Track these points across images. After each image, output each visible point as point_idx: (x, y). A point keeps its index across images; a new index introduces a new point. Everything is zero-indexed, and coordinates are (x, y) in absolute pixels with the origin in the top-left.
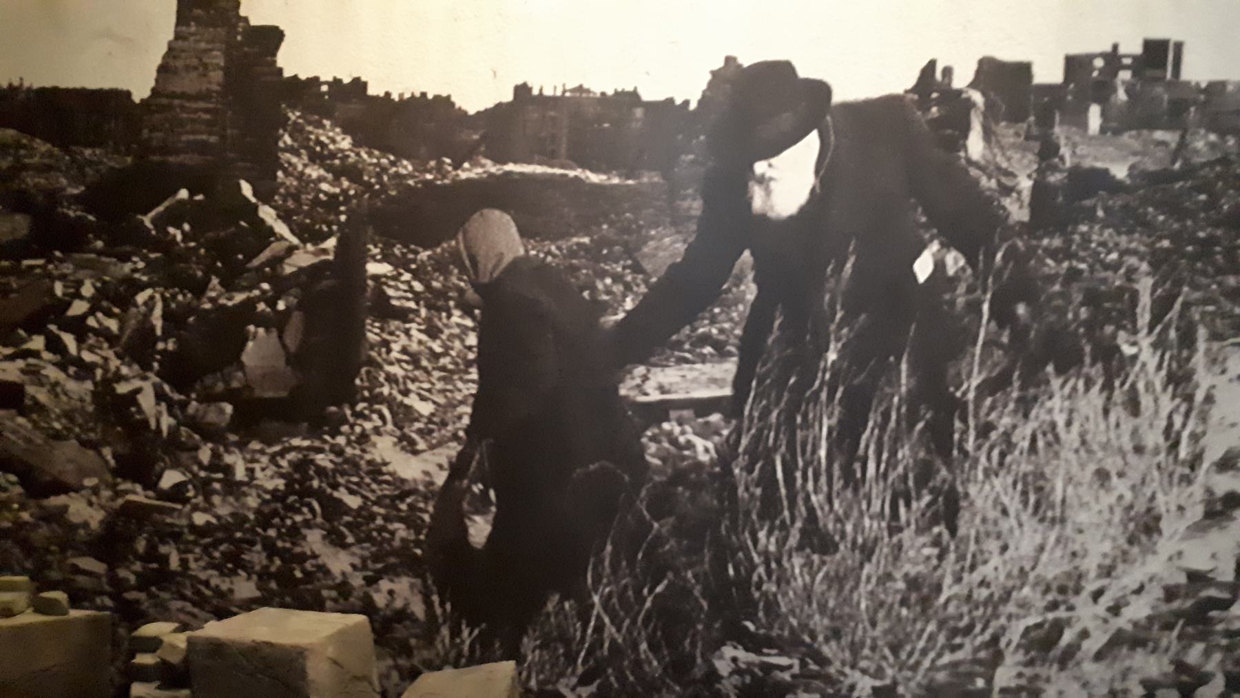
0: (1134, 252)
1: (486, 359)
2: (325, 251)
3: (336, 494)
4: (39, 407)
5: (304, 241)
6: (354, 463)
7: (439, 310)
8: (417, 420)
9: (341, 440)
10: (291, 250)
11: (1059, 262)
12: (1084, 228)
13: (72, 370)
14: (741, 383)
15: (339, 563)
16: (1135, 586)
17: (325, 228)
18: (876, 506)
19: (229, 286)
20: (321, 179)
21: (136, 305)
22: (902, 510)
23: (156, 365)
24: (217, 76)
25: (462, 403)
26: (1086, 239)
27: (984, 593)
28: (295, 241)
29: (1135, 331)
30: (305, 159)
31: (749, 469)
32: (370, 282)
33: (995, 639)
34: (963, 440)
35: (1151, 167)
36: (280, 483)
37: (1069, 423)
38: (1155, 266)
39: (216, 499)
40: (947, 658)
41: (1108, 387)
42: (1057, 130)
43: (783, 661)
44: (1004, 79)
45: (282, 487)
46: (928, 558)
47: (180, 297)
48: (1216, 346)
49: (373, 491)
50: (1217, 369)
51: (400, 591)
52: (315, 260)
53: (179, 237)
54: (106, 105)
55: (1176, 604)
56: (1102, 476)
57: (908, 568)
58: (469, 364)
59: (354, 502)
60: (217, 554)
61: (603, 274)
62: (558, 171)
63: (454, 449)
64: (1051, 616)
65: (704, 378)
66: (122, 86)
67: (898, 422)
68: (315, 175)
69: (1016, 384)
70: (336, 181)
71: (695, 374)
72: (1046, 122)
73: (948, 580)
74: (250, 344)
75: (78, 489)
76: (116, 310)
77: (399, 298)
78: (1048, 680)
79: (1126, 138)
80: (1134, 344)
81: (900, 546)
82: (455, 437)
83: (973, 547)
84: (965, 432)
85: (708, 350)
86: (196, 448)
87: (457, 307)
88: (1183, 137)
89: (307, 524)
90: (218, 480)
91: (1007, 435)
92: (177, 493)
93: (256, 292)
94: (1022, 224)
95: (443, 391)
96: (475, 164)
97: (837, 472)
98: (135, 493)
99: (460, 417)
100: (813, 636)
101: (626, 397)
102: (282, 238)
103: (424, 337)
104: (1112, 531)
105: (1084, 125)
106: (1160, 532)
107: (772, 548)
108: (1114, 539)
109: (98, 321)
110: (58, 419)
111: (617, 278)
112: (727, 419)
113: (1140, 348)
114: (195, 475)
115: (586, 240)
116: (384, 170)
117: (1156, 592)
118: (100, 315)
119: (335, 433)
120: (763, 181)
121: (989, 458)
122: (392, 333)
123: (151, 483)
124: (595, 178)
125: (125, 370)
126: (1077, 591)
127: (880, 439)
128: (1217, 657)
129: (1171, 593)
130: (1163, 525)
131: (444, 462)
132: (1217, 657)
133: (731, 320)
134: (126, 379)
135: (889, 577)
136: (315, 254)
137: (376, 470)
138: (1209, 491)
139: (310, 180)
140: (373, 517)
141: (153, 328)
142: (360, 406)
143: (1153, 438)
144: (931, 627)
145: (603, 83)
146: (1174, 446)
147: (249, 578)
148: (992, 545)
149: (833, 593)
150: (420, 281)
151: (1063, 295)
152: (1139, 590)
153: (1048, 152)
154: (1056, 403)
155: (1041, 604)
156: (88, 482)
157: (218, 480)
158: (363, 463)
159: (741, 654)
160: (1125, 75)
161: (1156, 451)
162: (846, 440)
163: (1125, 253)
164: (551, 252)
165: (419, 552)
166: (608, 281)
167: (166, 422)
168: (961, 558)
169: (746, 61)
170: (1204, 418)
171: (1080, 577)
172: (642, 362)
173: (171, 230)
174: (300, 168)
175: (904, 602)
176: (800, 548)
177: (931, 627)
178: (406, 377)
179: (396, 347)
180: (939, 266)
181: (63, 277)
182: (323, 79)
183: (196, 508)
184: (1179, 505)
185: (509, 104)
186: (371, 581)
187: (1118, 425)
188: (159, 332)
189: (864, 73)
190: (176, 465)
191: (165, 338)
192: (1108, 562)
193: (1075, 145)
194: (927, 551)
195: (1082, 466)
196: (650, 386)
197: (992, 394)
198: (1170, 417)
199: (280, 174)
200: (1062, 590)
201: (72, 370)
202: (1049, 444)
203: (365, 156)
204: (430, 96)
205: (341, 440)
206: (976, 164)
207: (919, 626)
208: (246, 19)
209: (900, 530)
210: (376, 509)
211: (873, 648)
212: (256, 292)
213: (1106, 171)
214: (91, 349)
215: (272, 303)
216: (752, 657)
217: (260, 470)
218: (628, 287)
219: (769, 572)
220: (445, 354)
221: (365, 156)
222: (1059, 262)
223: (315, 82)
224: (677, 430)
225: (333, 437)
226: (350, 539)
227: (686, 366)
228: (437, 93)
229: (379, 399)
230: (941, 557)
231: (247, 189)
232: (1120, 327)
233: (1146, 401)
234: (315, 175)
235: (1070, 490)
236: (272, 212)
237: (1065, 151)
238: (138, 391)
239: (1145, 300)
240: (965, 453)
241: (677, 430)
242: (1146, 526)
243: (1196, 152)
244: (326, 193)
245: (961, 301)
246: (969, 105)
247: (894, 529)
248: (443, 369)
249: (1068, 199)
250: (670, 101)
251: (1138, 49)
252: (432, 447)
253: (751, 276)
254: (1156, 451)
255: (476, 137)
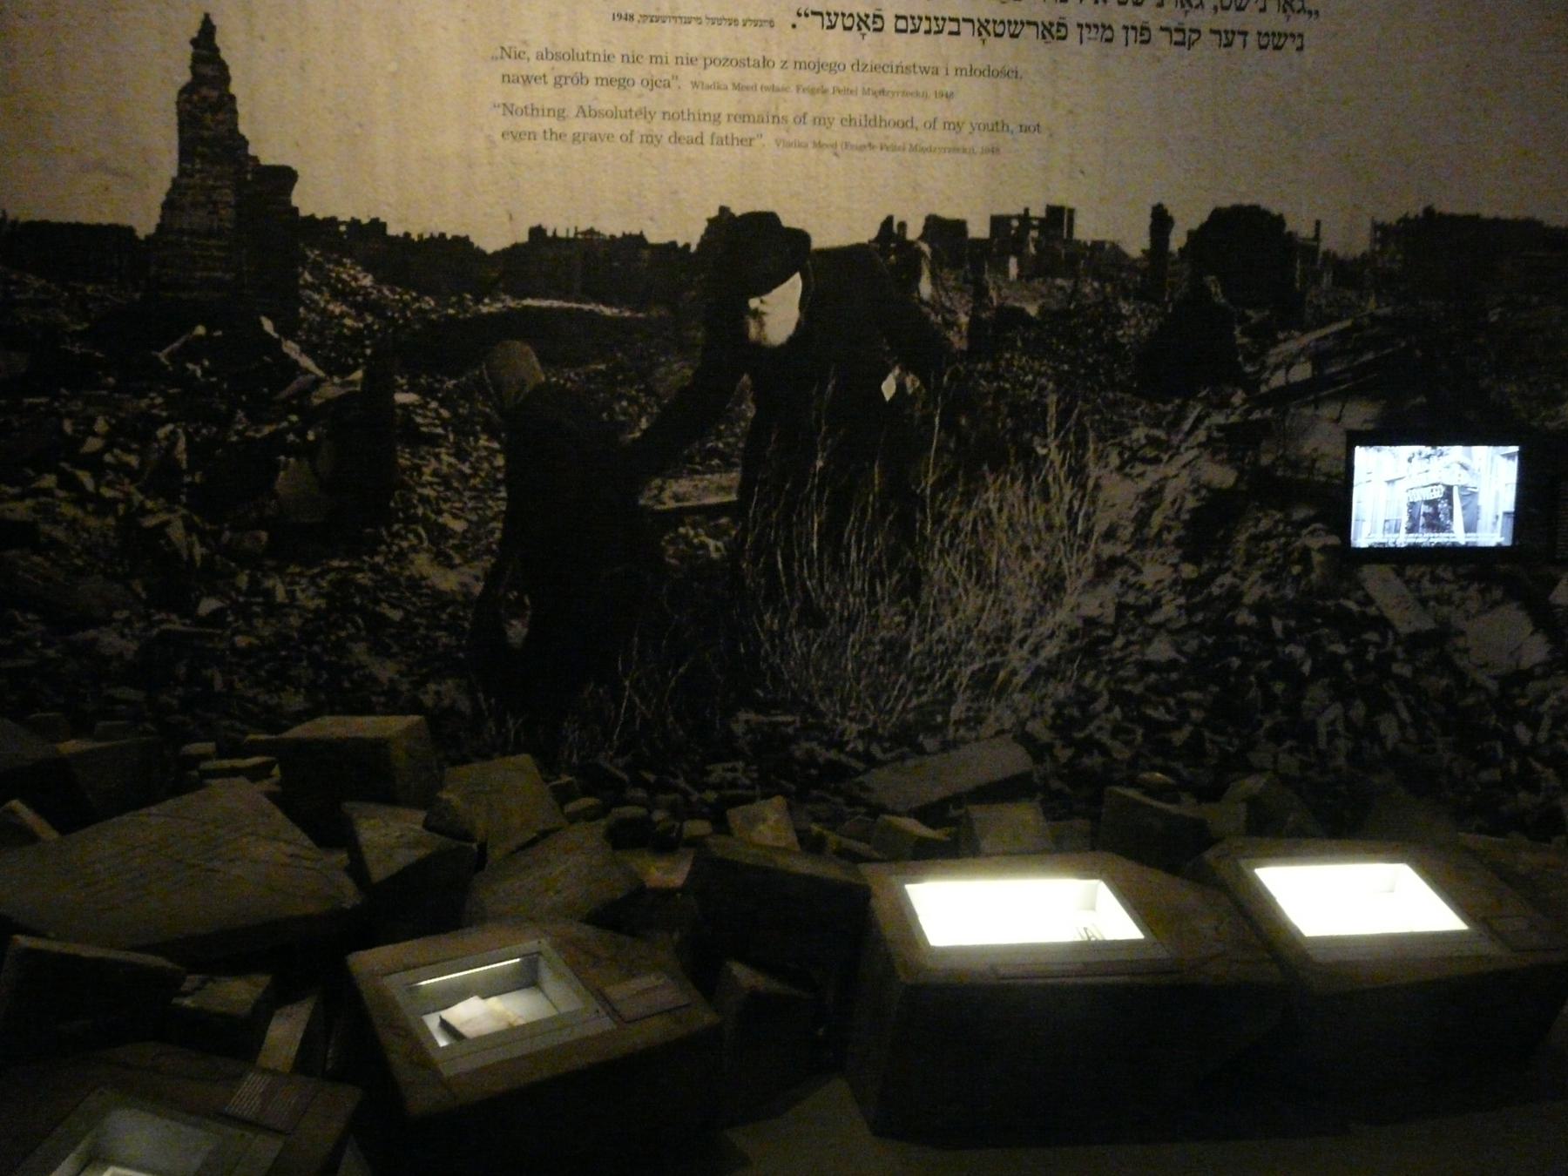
0: (1044, 375)
1: (513, 478)
2: (352, 383)
3: (441, 520)
4: (54, 542)
5: (330, 374)
6: (393, 580)
7: (466, 435)
8: (451, 537)
9: (379, 559)
10: (318, 382)
11: (990, 382)
12: (1008, 356)
13: (90, 507)
14: (745, 489)
15: (386, 671)
16: (1047, 633)
17: (351, 361)
18: (858, 585)
19: (255, 420)
20: (343, 315)
21: (156, 440)
22: (878, 588)
23: (183, 498)
24: (227, 213)
25: (494, 519)
26: (1009, 363)
27: (941, 648)
28: (321, 374)
29: (1046, 436)
30: (327, 296)
31: (755, 562)
32: (399, 411)
33: (950, 683)
34: (923, 527)
35: (1055, 307)
36: (321, 603)
37: (1000, 510)
38: (1059, 384)
39: (258, 623)
40: (914, 702)
41: (1027, 480)
42: (986, 276)
43: (789, 718)
44: (943, 231)
45: (323, 606)
46: (898, 625)
47: (204, 431)
48: (1101, 446)
49: (414, 604)
50: (1102, 464)
51: (446, 691)
52: (343, 392)
53: (199, 373)
54: (104, 244)
55: (1077, 643)
56: (1024, 549)
57: (883, 633)
58: (498, 483)
59: (396, 615)
60: (263, 673)
61: (621, 397)
62: (575, 305)
63: (488, 562)
64: (989, 662)
65: (713, 487)
66: (124, 220)
67: (873, 516)
68: (337, 311)
69: (961, 481)
70: (359, 317)
71: (705, 483)
72: (978, 270)
73: (914, 640)
74: (282, 474)
75: (108, 622)
76: (135, 446)
77: (427, 425)
78: (989, 710)
79: (1036, 283)
80: (1045, 446)
81: (877, 616)
82: (489, 551)
83: (931, 612)
84: (924, 522)
85: (715, 462)
86: (234, 574)
87: (484, 431)
88: (1076, 284)
89: (414, 549)
90: (258, 604)
91: (955, 521)
92: (216, 617)
93: (285, 424)
94: (962, 352)
95: (475, 509)
96: (494, 299)
97: (826, 560)
98: (169, 621)
99: (492, 532)
100: (811, 696)
101: (645, 506)
102: (307, 372)
103: (453, 460)
104: (1032, 592)
105: (1006, 272)
106: (1065, 590)
107: (775, 627)
108: (1034, 598)
109: (116, 457)
110: (79, 555)
111: (633, 401)
112: (735, 522)
113: (1049, 449)
114: (235, 602)
115: (602, 367)
116: (406, 305)
117: (1062, 635)
118: (117, 451)
119: (373, 553)
120: (757, 314)
121: (942, 541)
122: (422, 458)
123: (187, 611)
124: (608, 311)
125: (149, 504)
126: (1008, 640)
127: (860, 528)
128: (1104, 679)
129: (1073, 636)
130: (1068, 584)
131: (480, 573)
132: (1104, 679)
133: (735, 435)
134: (151, 512)
135: (869, 642)
136: (342, 385)
137: (416, 584)
138: (1097, 556)
139: (332, 316)
140: (415, 627)
141: (177, 462)
142: (396, 527)
143: (1059, 519)
144: (902, 678)
145: (612, 226)
146: (1074, 524)
147: (297, 692)
148: (946, 609)
149: (825, 660)
150: (447, 408)
151: (995, 408)
152: (1052, 636)
153: (980, 292)
154: (991, 494)
155: (983, 652)
156: (117, 615)
157: (258, 604)
158: (402, 580)
159: (752, 716)
160: (1034, 234)
161: (1061, 528)
162: (832, 535)
163: (1038, 374)
164: (570, 377)
165: (461, 655)
166: (625, 403)
167: (199, 551)
168: (924, 621)
169: (738, 211)
170: (1093, 502)
171: (1011, 628)
172: (657, 475)
173: (190, 366)
174: (322, 304)
175: (881, 661)
176: (798, 625)
177: (902, 678)
178: (437, 498)
179: (427, 470)
180: (901, 386)
181: (70, 415)
182: (341, 218)
183: (236, 632)
184: (1078, 567)
185: (524, 246)
186: (421, 683)
187: (1035, 509)
188: (184, 466)
189: (837, 219)
190: (213, 592)
191: (191, 471)
192: (1029, 616)
193: (1000, 289)
194: (897, 619)
195: (1010, 543)
196: (666, 495)
197: (942, 489)
198: (1071, 502)
199: (302, 310)
200: (998, 640)
201: (90, 507)
202: (986, 527)
203: (387, 292)
204: (449, 237)
205: (379, 559)
206: (927, 304)
207: (893, 678)
208: (255, 159)
209: (877, 603)
210: (417, 620)
211: (858, 699)
212: (285, 424)
213: (1022, 310)
214: (110, 485)
215: (301, 434)
216: (762, 718)
217: (300, 592)
218: (643, 410)
219: (773, 646)
220: (475, 475)
221: (387, 292)
222: (990, 382)
223: (332, 222)
224: (692, 533)
225: (372, 557)
226: (395, 649)
227: (697, 477)
228: (456, 233)
229: (415, 519)
230: (908, 624)
231: (268, 325)
232: (1035, 433)
233: (1054, 490)
234: (337, 311)
235: (1002, 562)
236: (297, 347)
237: (993, 294)
238: (167, 523)
239: (1052, 410)
240: (924, 539)
241: (692, 533)
242: (1053, 586)
243: (1086, 296)
244: (349, 328)
245: (917, 414)
246: (919, 253)
247: (872, 603)
248: (474, 488)
249: (996, 329)
250: (674, 244)
251: (1042, 214)
252: (466, 561)
253: (750, 396)
254: (1061, 528)
255: (494, 275)
